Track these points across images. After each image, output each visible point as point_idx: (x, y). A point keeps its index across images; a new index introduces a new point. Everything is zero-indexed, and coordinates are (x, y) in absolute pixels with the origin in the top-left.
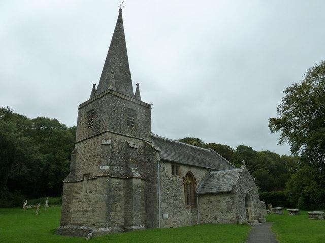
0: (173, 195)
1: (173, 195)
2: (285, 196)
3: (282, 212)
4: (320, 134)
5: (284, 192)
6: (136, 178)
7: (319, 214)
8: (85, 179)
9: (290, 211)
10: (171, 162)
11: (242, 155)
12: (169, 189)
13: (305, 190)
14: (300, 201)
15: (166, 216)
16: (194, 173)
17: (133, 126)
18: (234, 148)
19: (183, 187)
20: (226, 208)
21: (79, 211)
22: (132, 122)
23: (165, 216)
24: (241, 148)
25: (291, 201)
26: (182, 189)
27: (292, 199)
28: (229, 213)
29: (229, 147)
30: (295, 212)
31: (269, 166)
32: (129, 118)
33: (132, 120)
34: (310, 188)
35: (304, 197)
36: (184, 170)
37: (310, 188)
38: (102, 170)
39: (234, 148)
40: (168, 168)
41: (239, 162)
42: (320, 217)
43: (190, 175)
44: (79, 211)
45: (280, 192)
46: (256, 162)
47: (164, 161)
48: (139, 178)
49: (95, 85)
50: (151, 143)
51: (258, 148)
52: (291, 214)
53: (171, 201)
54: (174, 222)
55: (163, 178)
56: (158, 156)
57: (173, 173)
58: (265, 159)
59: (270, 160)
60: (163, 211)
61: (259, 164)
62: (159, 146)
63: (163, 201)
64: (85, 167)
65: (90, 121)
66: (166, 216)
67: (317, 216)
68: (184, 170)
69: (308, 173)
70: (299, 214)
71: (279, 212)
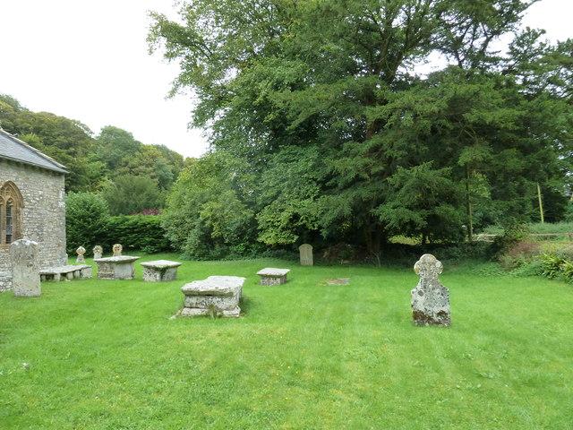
2: (162, 226)
3: (127, 270)
4: (265, 70)
5: (160, 218)
7: (222, 295)
9: (148, 267)
10: (66, 175)
11: (110, 144)
13: (205, 213)
14: (193, 238)
18: (96, 131)
24: (109, 132)
25: (173, 238)
27: (176, 233)
29: (78, 123)
30: (163, 271)
31: (161, 172)
34: (215, 205)
35: (202, 230)
37: (215, 205)
39: (96, 131)
41: (100, 160)
42: (227, 303)
45: (150, 218)
46: (135, 161)
51: (146, 136)
58: (153, 157)
59: (162, 160)
61: (141, 168)
67: (215, 300)
69: (219, 168)
70: (174, 278)
71: (118, 271)
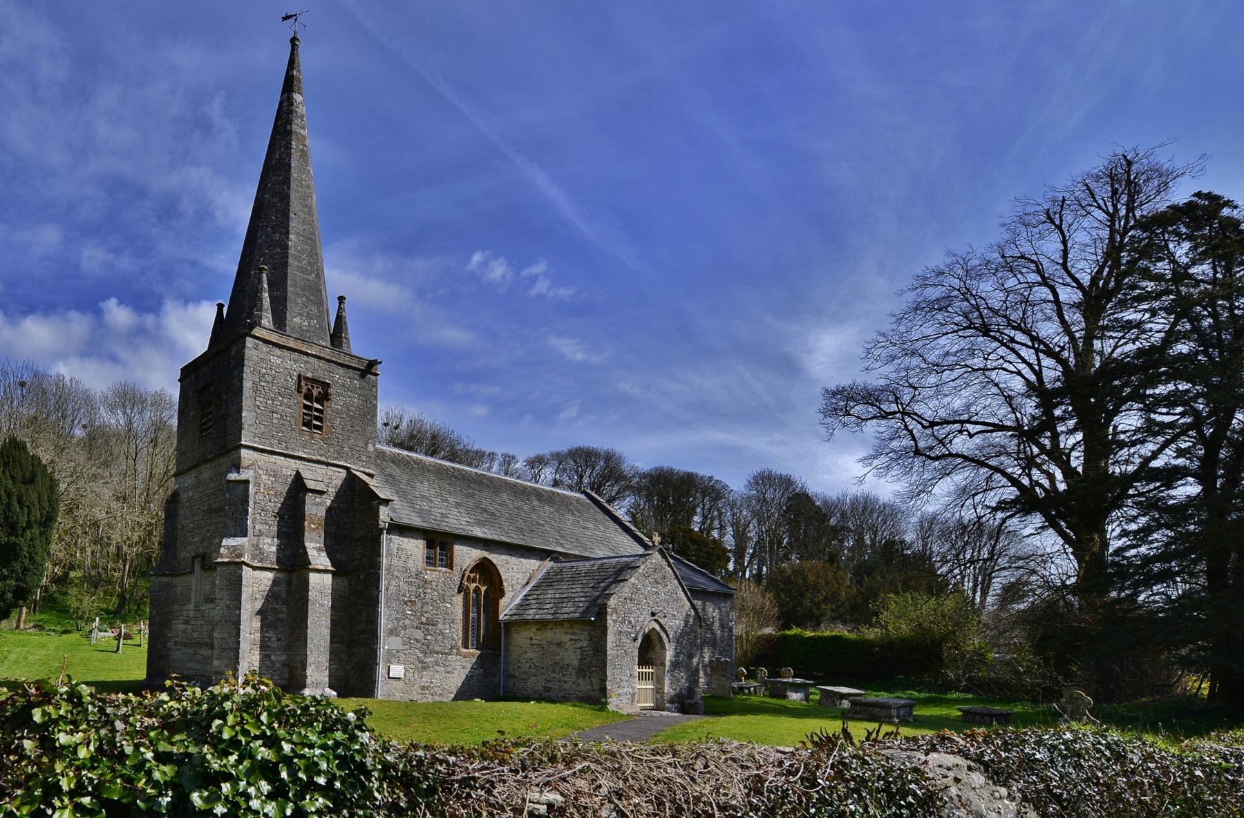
0: (424, 620)
1: (424, 620)
6: (319, 571)
8: (197, 568)
12: (413, 602)
15: (397, 670)
16: (495, 561)
17: (317, 427)
19: (459, 599)
20: (575, 663)
21: (185, 645)
22: (317, 418)
23: (394, 672)
26: (457, 605)
28: (584, 677)
32: (306, 407)
33: (317, 410)
36: (466, 556)
38: (228, 548)
40: (415, 548)
43: (485, 570)
44: (185, 645)
47: (400, 529)
48: (325, 571)
49: (220, 306)
50: (371, 476)
52: (131, 648)
53: (419, 634)
54: (423, 688)
55: (396, 573)
56: (384, 514)
57: (430, 561)
60: (392, 656)
62: (391, 481)
63: (392, 632)
64: (197, 539)
65: (204, 416)
66: (397, 670)
68: (466, 556)
